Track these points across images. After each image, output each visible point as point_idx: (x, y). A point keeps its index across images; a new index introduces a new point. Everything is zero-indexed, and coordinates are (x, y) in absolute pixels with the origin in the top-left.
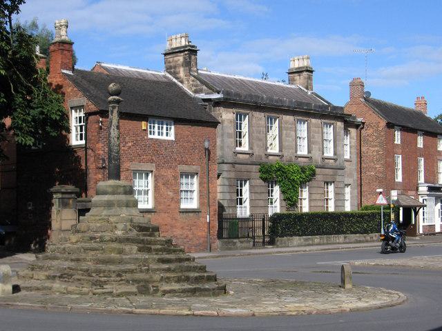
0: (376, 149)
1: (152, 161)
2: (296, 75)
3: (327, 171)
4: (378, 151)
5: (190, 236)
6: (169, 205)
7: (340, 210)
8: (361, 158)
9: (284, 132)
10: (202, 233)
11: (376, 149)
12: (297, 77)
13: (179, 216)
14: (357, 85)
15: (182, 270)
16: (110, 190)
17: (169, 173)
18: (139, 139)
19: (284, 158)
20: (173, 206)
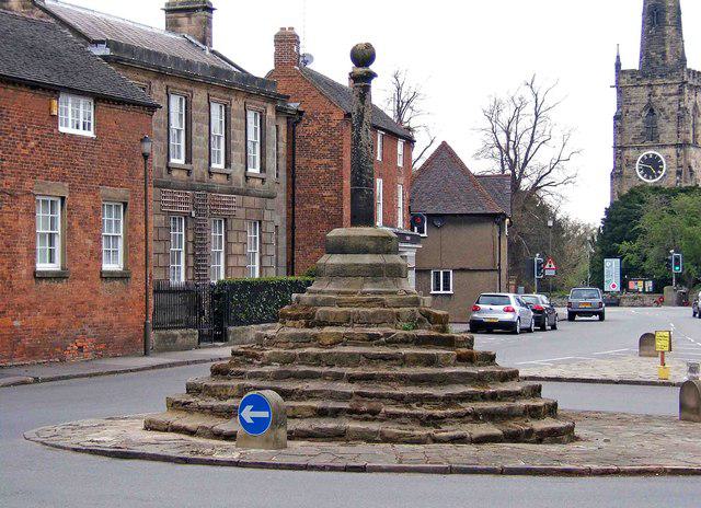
0: (325, 161)
1: (63, 178)
2: (183, 14)
3: (250, 201)
4: (327, 166)
5: (116, 325)
6: (88, 265)
7: (238, 276)
8: (293, 177)
9: (194, 125)
10: (134, 318)
11: (325, 161)
12: (183, 20)
13: (104, 288)
14: (286, 42)
15: (507, 415)
16: (371, 244)
17: (85, 202)
18: (45, 133)
19: (193, 175)
20: (92, 267)
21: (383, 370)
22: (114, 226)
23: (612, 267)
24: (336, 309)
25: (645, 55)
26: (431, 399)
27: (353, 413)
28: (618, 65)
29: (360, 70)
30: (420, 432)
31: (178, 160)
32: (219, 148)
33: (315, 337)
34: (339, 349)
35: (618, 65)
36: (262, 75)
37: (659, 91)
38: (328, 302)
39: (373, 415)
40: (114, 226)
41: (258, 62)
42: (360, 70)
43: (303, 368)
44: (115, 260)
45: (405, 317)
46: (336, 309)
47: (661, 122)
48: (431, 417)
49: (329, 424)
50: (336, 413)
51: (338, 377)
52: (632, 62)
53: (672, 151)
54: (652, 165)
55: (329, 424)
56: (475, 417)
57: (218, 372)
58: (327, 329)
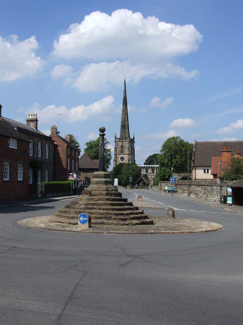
14: (54, 129)
21: (118, 207)
22: (20, 171)
23: (116, 181)
24: (97, 192)
25: (121, 135)
26: (123, 214)
27: (106, 218)
28: (115, 137)
29: (102, 133)
30: (122, 222)
31: (40, 156)
32: (40, 153)
33: (93, 199)
34: (98, 202)
35: (115, 137)
36: (48, 136)
37: (124, 143)
38: (94, 190)
39: (110, 218)
40: (20, 171)
41: (48, 133)
42: (102, 133)
43: (91, 207)
44: (7, 178)
45: (113, 195)
46: (97, 192)
47: (124, 149)
48: (124, 219)
49: (100, 221)
50: (101, 218)
51: (100, 209)
52: (118, 136)
53: (127, 156)
54: (122, 159)
55: (100, 221)
56: (133, 219)
57: (67, 207)
58: (95, 197)
